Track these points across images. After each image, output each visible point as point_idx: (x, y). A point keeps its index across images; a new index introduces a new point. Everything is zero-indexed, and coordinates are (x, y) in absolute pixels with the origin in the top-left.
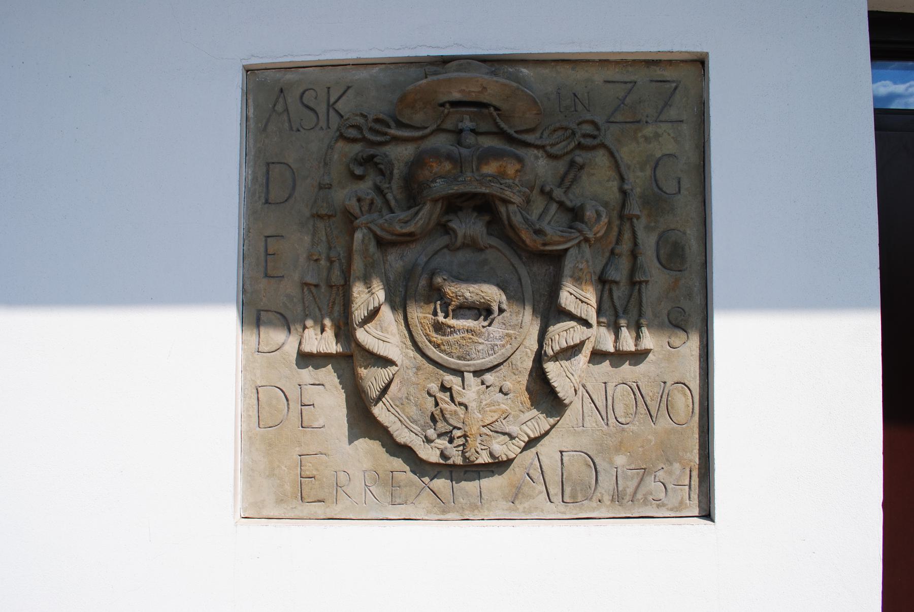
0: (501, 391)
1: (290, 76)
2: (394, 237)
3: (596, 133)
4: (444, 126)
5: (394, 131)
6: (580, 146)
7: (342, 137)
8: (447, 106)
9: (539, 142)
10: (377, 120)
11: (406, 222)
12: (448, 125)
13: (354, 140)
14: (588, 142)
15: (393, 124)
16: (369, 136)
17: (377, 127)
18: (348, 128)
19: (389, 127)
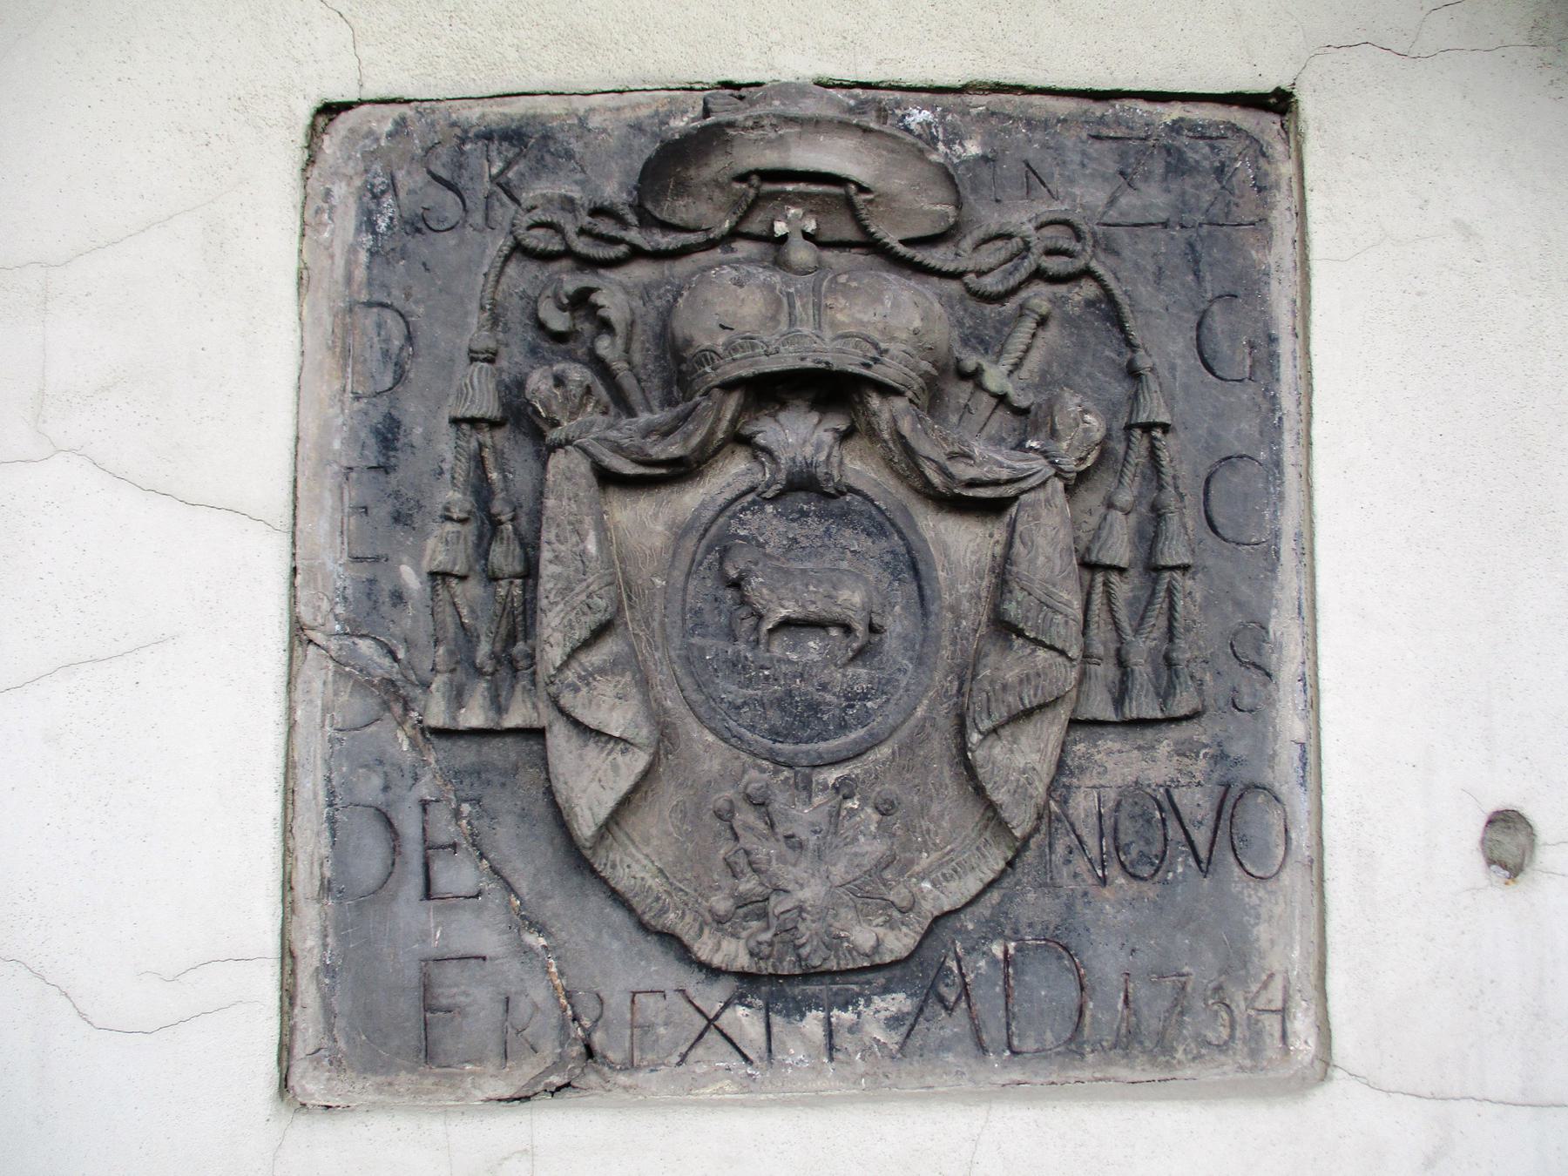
0: (424, 264)
1: (311, 786)
2: (641, 470)
3: (1016, 243)
4: (745, 228)
5: (634, 235)
6: (1039, 274)
7: (520, 250)
8: (755, 180)
9: (950, 267)
10: (598, 211)
11: (666, 434)
12: (755, 225)
13: (546, 257)
14: (1055, 265)
15: (632, 218)
16: (581, 245)
17: (606, 227)
18: (530, 227)
19: (625, 225)
